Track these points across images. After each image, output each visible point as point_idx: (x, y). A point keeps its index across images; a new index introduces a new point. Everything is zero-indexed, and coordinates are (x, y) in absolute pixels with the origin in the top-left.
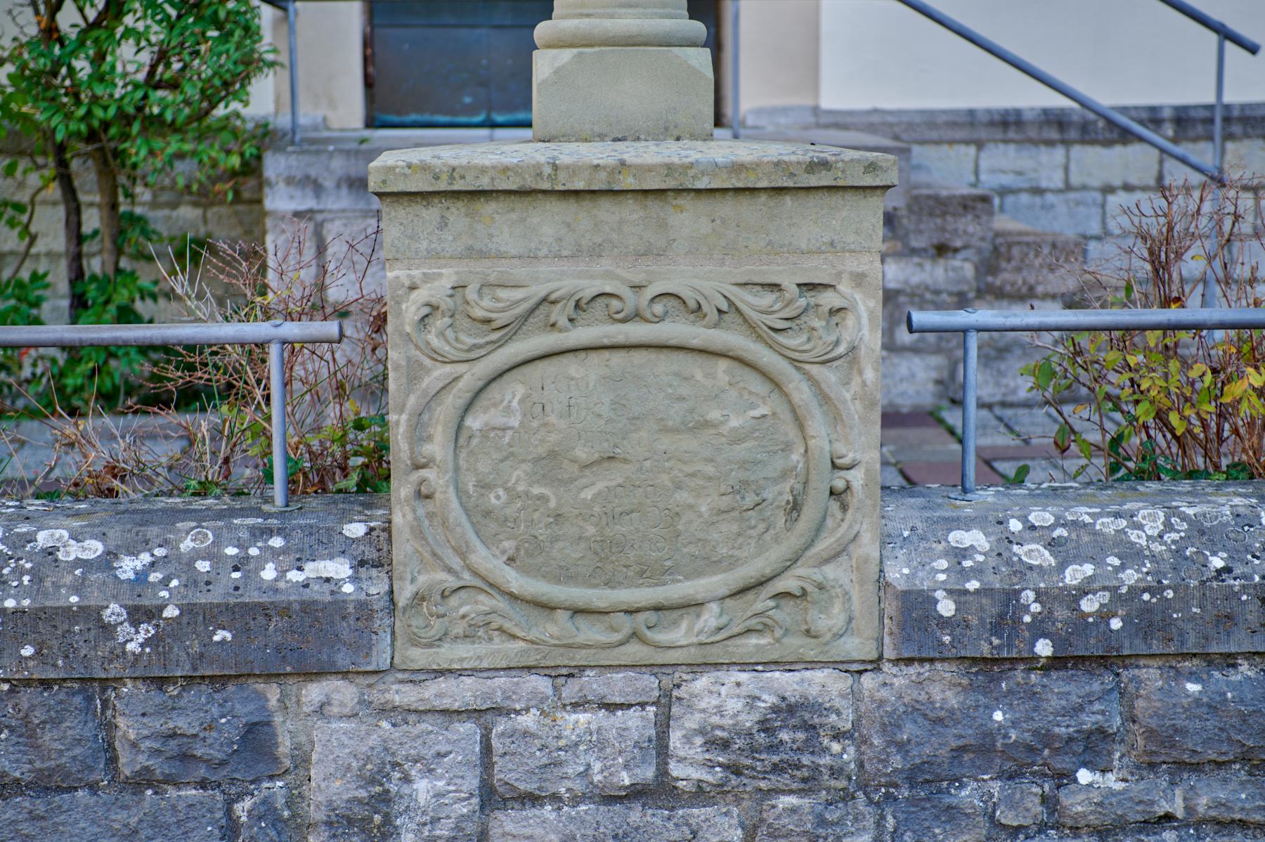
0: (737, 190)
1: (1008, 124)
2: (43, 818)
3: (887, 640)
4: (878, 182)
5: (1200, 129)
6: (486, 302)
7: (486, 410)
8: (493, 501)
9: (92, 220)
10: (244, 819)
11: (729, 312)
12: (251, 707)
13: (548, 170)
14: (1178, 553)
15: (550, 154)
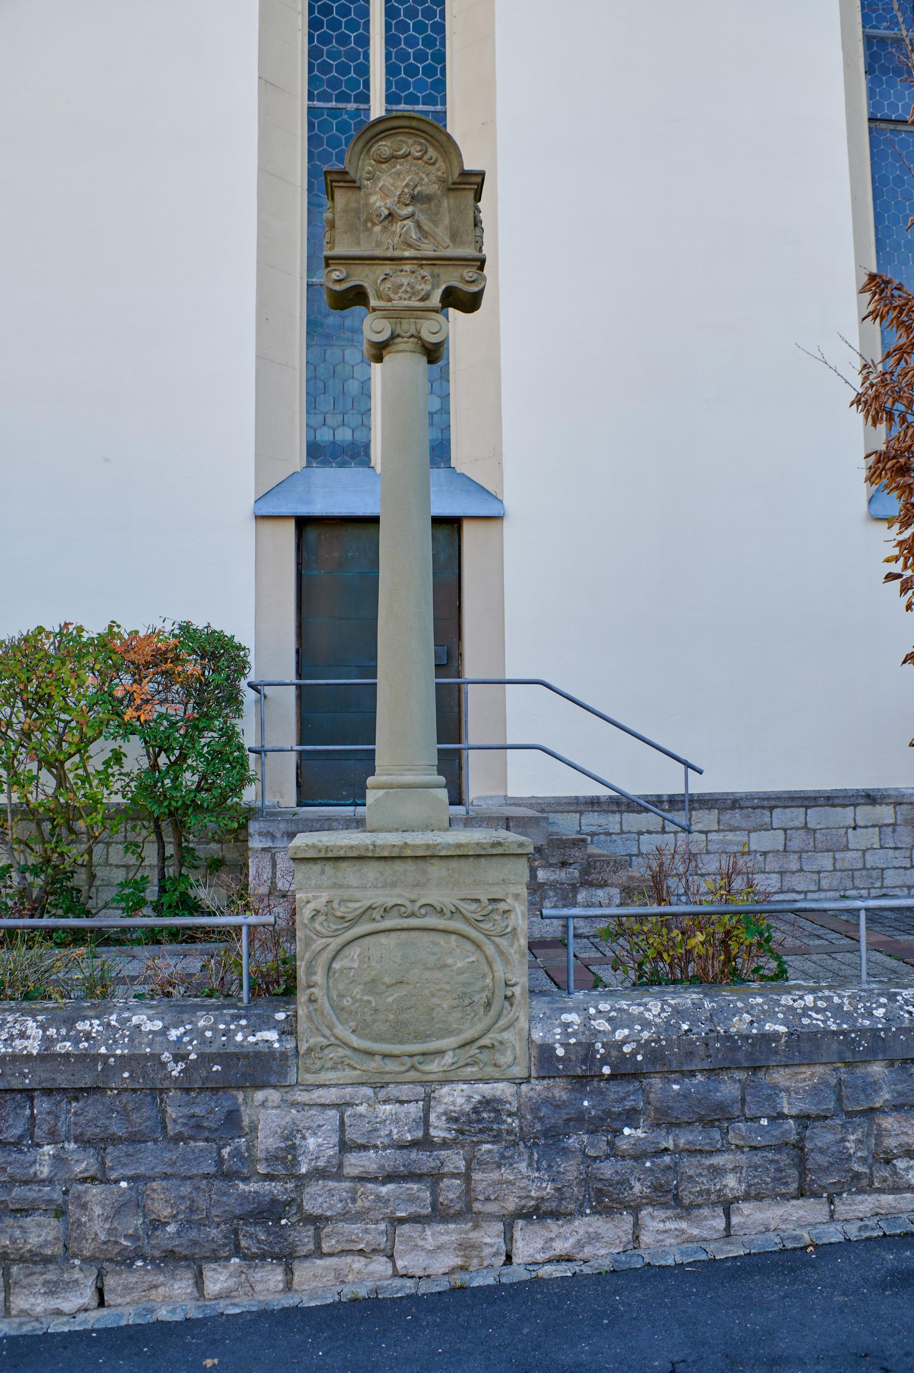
0: (459, 856)
1: (594, 803)
2: (132, 1155)
3: (533, 1068)
4: (524, 852)
5: (680, 805)
6: (342, 909)
7: (342, 959)
8: (345, 1003)
9: (170, 850)
10: (226, 1157)
11: (456, 913)
12: (230, 1103)
13: (371, 847)
14: (667, 1023)
15: (373, 839)
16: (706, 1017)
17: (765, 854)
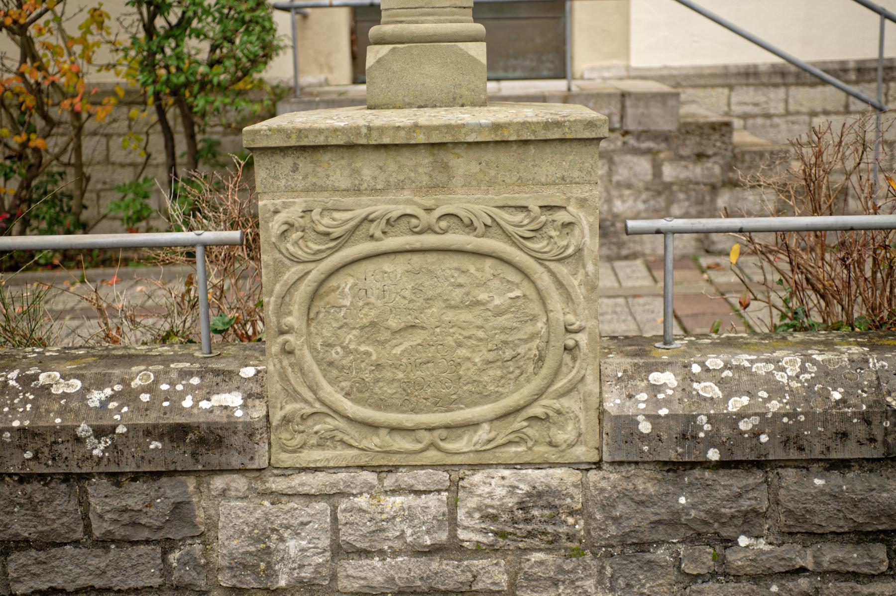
0: (496, 142)
2: (45, 563)
3: (605, 448)
11: (492, 227)
13: (364, 131)
16: (870, 382)
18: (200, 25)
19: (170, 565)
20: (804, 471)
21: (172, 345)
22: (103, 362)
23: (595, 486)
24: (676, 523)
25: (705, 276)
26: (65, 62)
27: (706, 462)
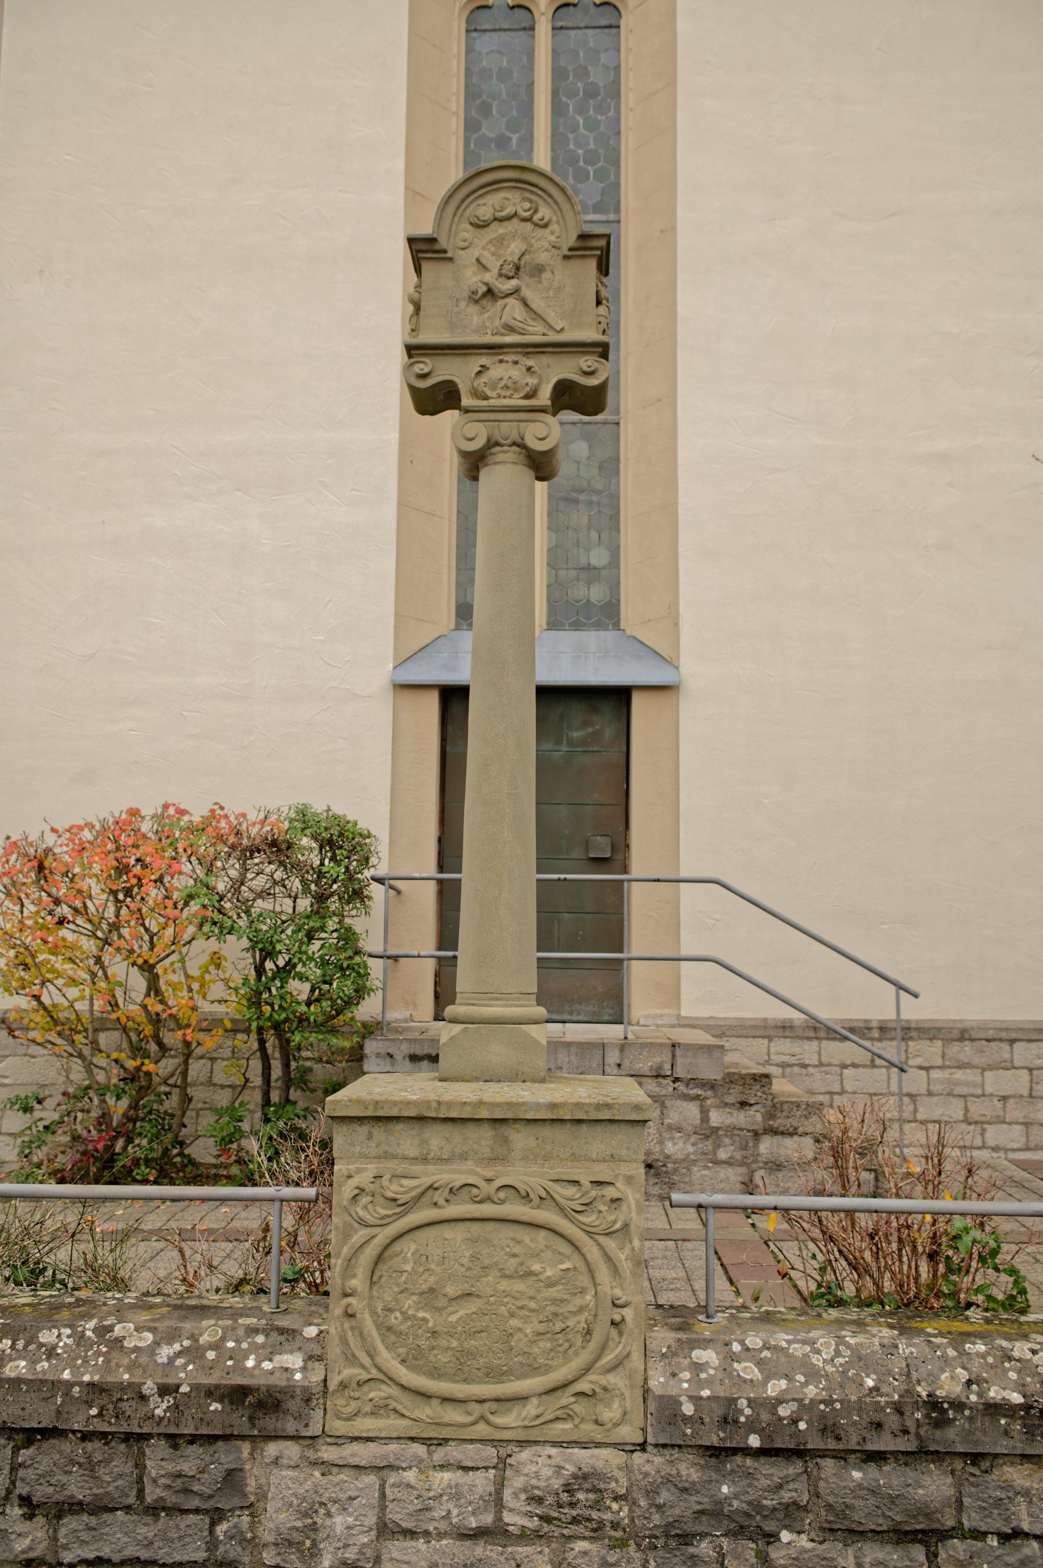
0: (552, 1120)
1: (785, 1028)
2: (95, 1529)
3: (649, 1429)
11: (547, 1199)
13: (434, 1105)
16: (901, 1369)
17: (1004, 1099)
18: (303, 970)
19: (217, 1538)
20: (842, 1462)
21: (242, 1296)
22: (176, 1314)
23: (639, 1470)
24: (718, 1514)
25: (750, 1221)
26: (183, 998)
27: (747, 1448)
